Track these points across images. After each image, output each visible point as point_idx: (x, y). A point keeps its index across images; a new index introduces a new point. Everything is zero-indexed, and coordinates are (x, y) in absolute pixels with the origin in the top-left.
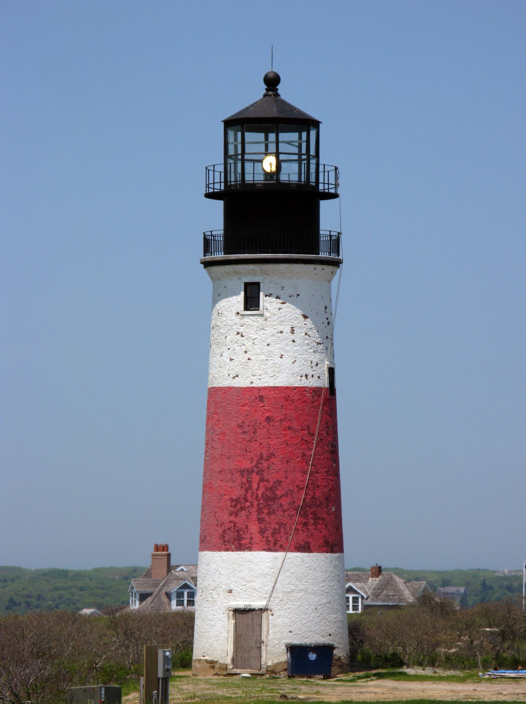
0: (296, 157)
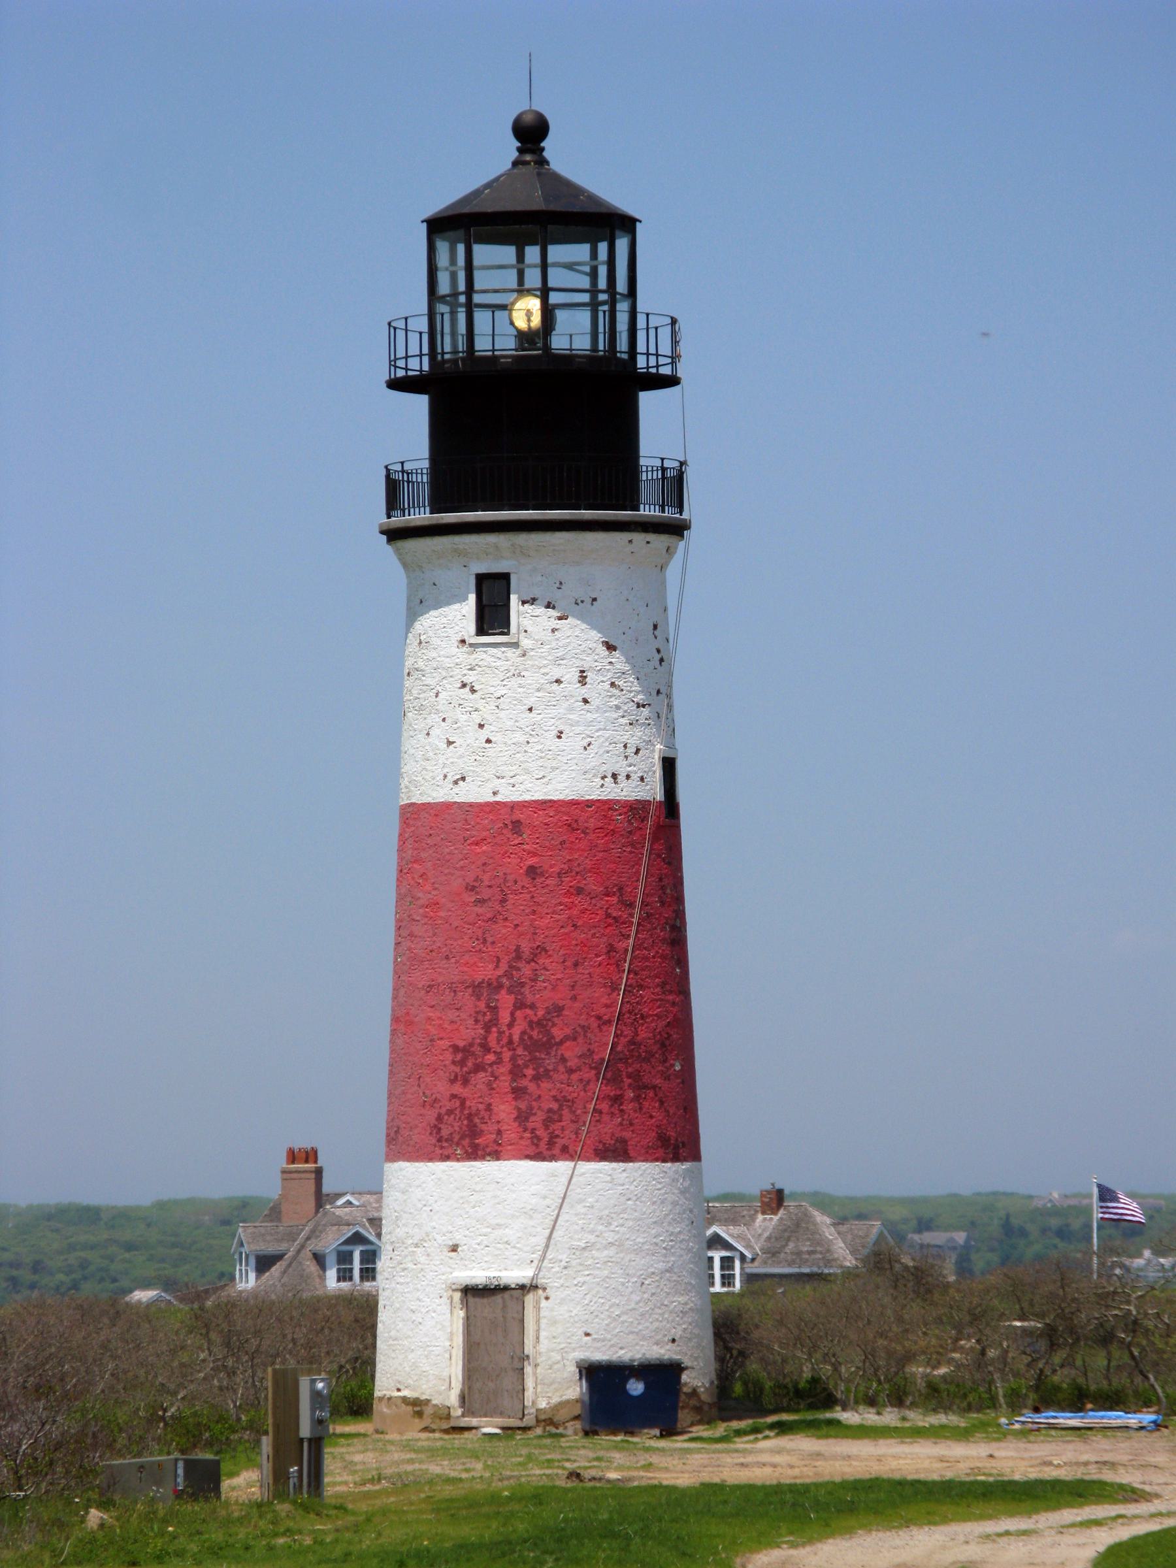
0: (585, 298)
